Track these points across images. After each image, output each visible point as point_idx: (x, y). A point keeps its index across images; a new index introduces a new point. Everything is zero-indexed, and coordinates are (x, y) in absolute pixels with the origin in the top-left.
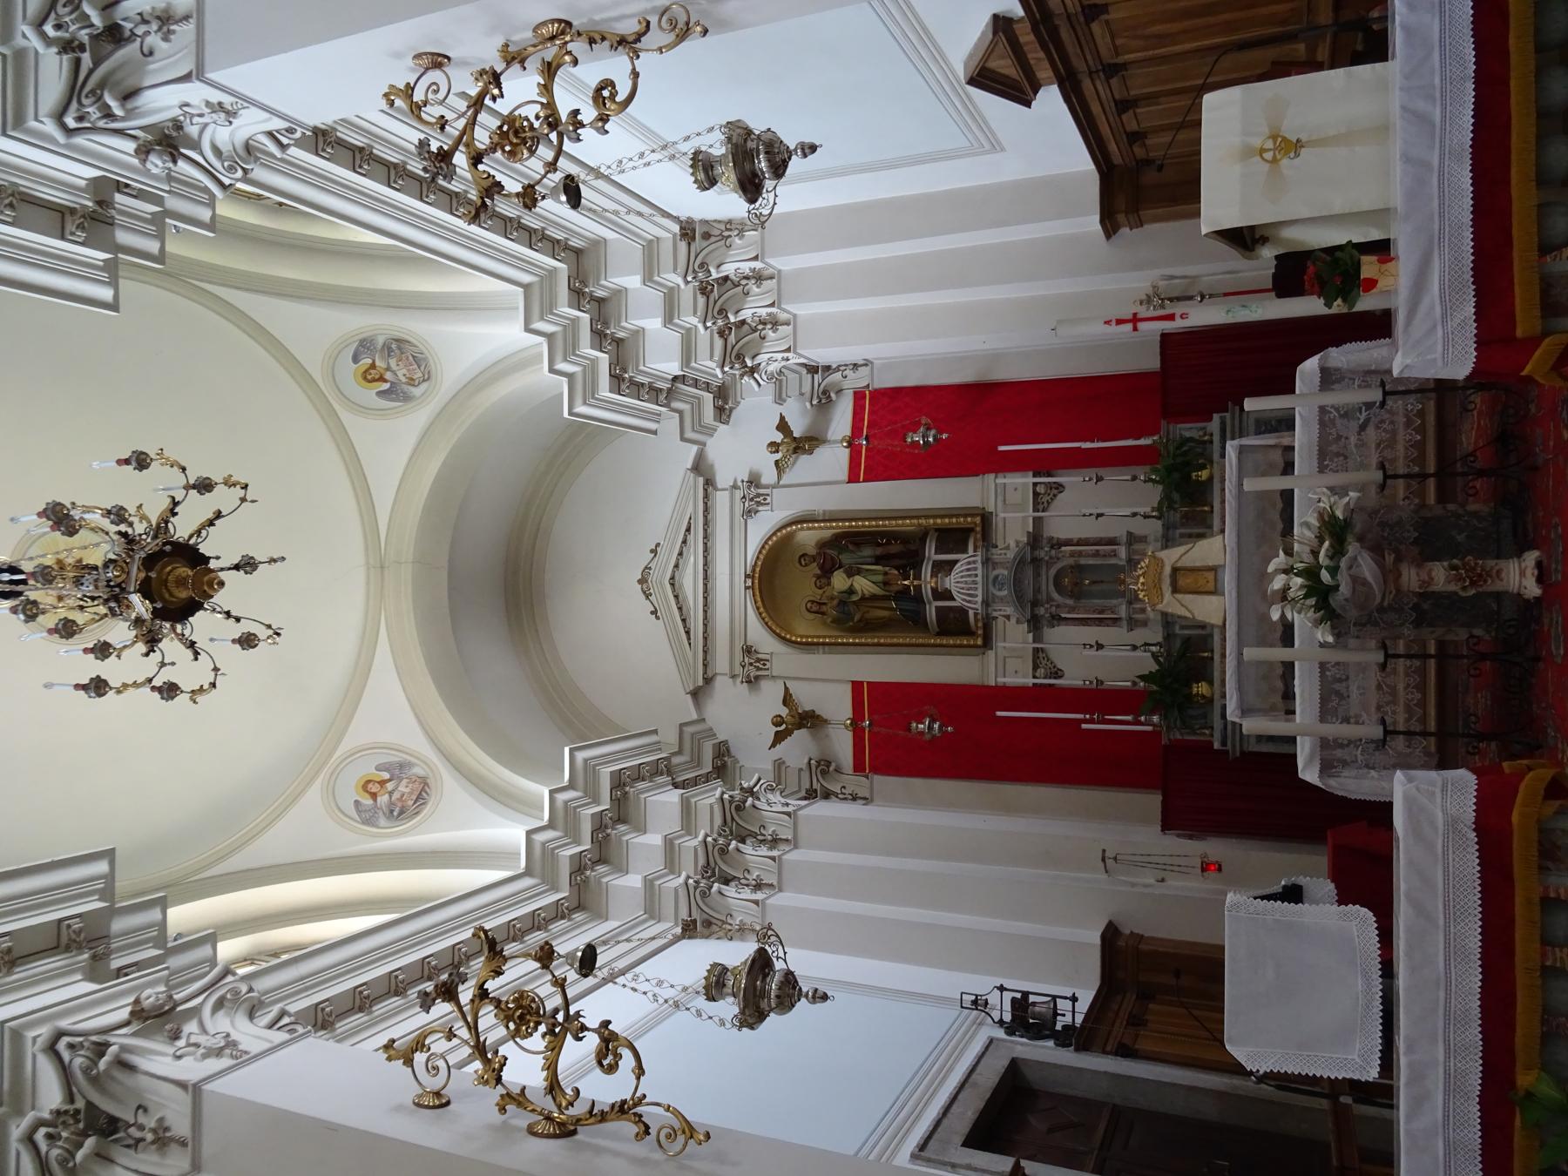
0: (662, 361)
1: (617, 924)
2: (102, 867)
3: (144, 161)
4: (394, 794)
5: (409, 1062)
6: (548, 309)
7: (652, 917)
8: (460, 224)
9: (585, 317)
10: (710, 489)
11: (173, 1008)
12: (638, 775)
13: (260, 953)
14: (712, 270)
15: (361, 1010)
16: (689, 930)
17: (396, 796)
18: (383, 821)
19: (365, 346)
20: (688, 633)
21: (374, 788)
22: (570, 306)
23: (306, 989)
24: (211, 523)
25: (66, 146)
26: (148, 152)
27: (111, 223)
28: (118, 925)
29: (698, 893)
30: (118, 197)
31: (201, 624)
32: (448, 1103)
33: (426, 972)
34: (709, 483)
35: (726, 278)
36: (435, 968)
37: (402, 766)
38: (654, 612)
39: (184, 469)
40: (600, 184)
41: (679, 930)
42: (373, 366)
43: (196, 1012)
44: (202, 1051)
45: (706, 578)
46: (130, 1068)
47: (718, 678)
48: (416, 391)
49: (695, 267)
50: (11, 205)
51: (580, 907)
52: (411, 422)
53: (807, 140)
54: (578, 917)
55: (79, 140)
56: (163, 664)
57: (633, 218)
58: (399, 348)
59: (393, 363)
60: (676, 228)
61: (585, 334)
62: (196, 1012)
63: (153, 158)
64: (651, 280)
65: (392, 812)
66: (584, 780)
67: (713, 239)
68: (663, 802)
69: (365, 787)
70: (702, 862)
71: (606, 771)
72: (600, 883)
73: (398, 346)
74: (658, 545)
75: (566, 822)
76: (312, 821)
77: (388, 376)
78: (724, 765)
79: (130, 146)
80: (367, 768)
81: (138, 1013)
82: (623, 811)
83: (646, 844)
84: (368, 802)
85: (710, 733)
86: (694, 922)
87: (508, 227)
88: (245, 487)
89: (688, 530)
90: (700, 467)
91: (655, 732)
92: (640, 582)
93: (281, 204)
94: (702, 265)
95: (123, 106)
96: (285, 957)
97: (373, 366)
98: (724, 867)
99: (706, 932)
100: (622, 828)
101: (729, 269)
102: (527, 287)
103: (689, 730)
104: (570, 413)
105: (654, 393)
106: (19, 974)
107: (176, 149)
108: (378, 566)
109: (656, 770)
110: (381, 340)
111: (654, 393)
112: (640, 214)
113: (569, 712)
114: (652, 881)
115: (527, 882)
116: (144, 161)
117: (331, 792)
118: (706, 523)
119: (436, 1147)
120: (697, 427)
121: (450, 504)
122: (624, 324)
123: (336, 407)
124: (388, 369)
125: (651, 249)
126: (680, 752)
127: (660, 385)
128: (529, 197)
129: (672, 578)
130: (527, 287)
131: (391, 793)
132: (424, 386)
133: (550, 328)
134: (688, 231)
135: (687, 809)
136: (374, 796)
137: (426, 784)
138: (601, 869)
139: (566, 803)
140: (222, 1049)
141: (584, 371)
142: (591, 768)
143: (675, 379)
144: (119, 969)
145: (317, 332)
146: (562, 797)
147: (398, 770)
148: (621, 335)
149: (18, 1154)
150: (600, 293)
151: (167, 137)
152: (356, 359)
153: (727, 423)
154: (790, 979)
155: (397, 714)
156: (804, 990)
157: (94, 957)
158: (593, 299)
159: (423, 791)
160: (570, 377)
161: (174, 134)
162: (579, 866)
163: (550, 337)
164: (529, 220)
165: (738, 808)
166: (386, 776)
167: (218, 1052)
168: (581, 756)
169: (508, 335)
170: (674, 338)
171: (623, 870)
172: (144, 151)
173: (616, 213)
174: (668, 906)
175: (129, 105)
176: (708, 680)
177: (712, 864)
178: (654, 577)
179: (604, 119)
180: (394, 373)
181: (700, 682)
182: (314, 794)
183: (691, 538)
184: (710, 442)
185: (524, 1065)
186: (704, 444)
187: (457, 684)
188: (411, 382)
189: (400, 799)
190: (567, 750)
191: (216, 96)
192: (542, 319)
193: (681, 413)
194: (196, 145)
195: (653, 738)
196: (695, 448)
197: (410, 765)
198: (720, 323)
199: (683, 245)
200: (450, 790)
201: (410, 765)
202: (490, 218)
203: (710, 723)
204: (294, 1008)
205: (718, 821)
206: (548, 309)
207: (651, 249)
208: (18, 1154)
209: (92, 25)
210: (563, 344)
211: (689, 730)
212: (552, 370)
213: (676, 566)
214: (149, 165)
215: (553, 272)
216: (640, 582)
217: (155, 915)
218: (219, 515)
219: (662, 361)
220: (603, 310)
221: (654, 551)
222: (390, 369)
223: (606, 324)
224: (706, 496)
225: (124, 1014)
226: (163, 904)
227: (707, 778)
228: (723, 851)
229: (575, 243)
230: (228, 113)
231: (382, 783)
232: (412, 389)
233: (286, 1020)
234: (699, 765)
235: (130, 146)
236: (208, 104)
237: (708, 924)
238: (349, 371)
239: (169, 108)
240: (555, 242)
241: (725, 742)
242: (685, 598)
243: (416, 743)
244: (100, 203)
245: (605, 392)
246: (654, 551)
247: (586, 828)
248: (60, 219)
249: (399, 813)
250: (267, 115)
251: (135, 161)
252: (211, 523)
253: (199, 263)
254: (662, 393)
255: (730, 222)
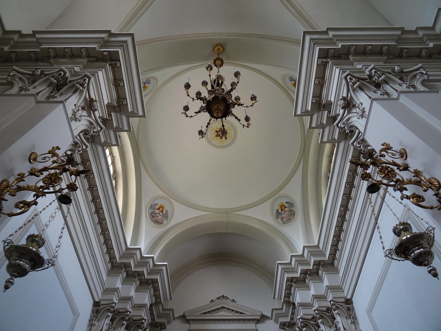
0: (300, 296)
1: (105, 279)
2: (141, 113)
3: (341, 99)
4: (158, 215)
5: (49, 152)
6: (312, 254)
7: (104, 291)
8: (350, 157)
9: (311, 267)
10: (256, 321)
11: (92, 110)
12: (156, 289)
13: (116, 175)
14: (336, 312)
15: (89, 187)
16: (96, 304)
17: (158, 215)
18: (151, 211)
19: (291, 205)
20: (205, 313)
21: (161, 209)
22: (314, 261)
23: (99, 172)
24: (236, 118)
25: (341, 77)
26: (344, 100)
27: (319, 110)
28: (124, 118)
29: (109, 308)
30: (326, 112)
31: (206, 116)
32: (30, 162)
33: (98, 209)
34: (258, 321)
35: (334, 318)
36: (99, 212)
37: (167, 217)
38: (212, 301)
39: (252, 106)
40: (379, 200)
41: (97, 300)
42: (286, 207)
43: (90, 116)
44: (76, 111)
45: (224, 320)
46: (75, 92)
47: (189, 325)
48: (279, 220)
49: (336, 305)
50: (320, 82)
51: (113, 266)
52: (270, 219)
53: (438, 271)
54: (109, 265)
55: (344, 82)
56: (193, 99)
57: (370, 209)
58: (292, 214)
59: (287, 213)
60: (349, 297)
61: (306, 268)
62: (90, 116)
63: (342, 101)
64: (329, 289)
65: (153, 213)
66: (156, 270)
67: (348, 312)
68: (146, 298)
69: (161, 207)
70: (121, 310)
71: (158, 277)
72: (120, 273)
73: (292, 214)
74: (235, 302)
75: (142, 262)
76: (152, 192)
77: (283, 212)
78: (157, 327)
79: (345, 95)
80: (167, 207)
81: (92, 100)
82: (145, 283)
83: (131, 291)
84: (157, 207)
85: (169, 322)
86: (99, 306)
87: (353, 173)
88: (248, 127)
89: (241, 313)
90: (263, 318)
91: (171, 299)
92: (223, 296)
93: (329, 178)
94: (337, 307)
95: (357, 86)
96: (114, 182)
97: (286, 207)
98: (117, 319)
99: (95, 311)
100: (138, 283)
101: (338, 319)
102: (318, 246)
103: (171, 313)
104: (278, 264)
105: (288, 295)
106: (112, 87)
107: (347, 107)
108: (227, 212)
109: (157, 296)
110: (293, 209)
111: (288, 295)
112: (373, 211)
113: (180, 273)
114: (117, 291)
115: (124, 248)
116: (341, 99)
117: (161, 197)
118: (244, 320)
119: (11, 147)
120: (277, 315)
121: (245, 233)
122: (311, 282)
123: (272, 199)
124: (285, 212)
125: (339, 289)
126: (163, 309)
127: (291, 297)
128: (366, 177)
129: (224, 308)
130: (318, 246)
131: (159, 214)
132: (281, 222)
133: (305, 255)
134: (349, 302)
135: (142, 306)
136: (159, 209)
137: (161, 224)
138: (125, 274)
139: (149, 262)
140: (75, 116)
141: (293, 268)
142: (159, 272)
143: (294, 304)
144: (111, 115)
145: (294, 192)
146: (151, 261)
147: (166, 216)
148: (307, 281)
149: (58, 68)
150: (320, 272)
151: (350, 104)
152: (287, 203)
153: (280, 328)
154: (22, 273)
155: (182, 216)
156: (15, 279)
157: (115, 107)
158: (318, 269)
159: (158, 223)
160: (290, 263)
161: (351, 106)
162: (127, 266)
163: (303, 255)
164: (357, 178)
165: (139, 326)
166: (164, 213)
167: (74, 114)
168: (164, 268)
169: (299, 244)
170: (309, 300)
171: (123, 283)
172: (344, 99)
173: (371, 202)
174: (107, 297)
175: (358, 89)
176: (188, 321)
177: (120, 314)
178: (224, 300)
179: (408, 198)
180: (284, 213)
181: (187, 318)
182: (160, 193)
183: (238, 314)
184: (272, 321)
185: (31, 181)
186: (271, 319)
187: (192, 234)
188: (282, 218)
189: (157, 216)
190: (166, 263)
191: (367, 110)
192: (308, 252)
193: (282, 309)
194: (349, 113)
195: (169, 298)
196: (270, 315)
197: (167, 220)
198: (317, 316)
199: (343, 300)
200: (158, 230)
201: (167, 220)
202: (334, 249)
203: (173, 322)
204: (88, 149)
205: (135, 318)
206: (312, 254)
207: (339, 289)
208: (58, 68)
209: (379, 79)
210: (301, 260)
211: (171, 313)
212: (292, 256)
213: (228, 309)
214: (340, 101)
215: (324, 255)
216: (223, 296)
217: (126, 128)
218: (239, 120)
219: (300, 296)
220: (313, 274)
221: (233, 301)
222: (285, 212)
223: (310, 275)
224: (253, 320)
225: (93, 96)
226: (129, 131)
227: (153, 319)
228: (123, 319)
229: (336, 262)
230: (362, 114)
231: (162, 212)
232: (280, 219)
233: (84, 147)
234: (158, 317)
235: (345, 95)
236: (364, 109)
237: (98, 312)
238: (283, 201)
239: (359, 101)
240: (339, 236)
241: (166, 328)
242: (217, 313)
243: (173, 222)
244: (324, 105)
245: (286, 276)
246: (233, 301)
247: (139, 269)
248: (318, 96)
249: (153, 216)
250: (364, 125)
251: (341, 98)
252: (236, 118)
253: (308, 159)
254: (289, 302)
255: (356, 318)
